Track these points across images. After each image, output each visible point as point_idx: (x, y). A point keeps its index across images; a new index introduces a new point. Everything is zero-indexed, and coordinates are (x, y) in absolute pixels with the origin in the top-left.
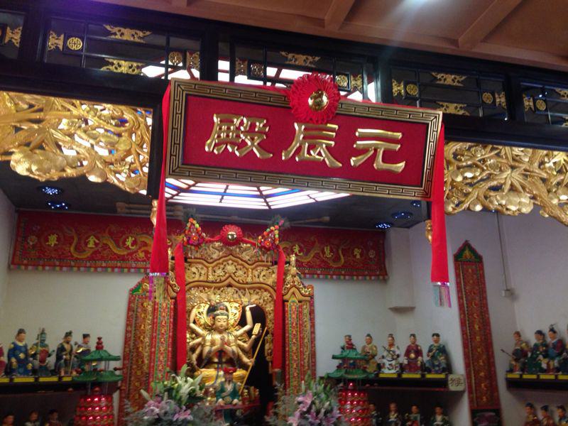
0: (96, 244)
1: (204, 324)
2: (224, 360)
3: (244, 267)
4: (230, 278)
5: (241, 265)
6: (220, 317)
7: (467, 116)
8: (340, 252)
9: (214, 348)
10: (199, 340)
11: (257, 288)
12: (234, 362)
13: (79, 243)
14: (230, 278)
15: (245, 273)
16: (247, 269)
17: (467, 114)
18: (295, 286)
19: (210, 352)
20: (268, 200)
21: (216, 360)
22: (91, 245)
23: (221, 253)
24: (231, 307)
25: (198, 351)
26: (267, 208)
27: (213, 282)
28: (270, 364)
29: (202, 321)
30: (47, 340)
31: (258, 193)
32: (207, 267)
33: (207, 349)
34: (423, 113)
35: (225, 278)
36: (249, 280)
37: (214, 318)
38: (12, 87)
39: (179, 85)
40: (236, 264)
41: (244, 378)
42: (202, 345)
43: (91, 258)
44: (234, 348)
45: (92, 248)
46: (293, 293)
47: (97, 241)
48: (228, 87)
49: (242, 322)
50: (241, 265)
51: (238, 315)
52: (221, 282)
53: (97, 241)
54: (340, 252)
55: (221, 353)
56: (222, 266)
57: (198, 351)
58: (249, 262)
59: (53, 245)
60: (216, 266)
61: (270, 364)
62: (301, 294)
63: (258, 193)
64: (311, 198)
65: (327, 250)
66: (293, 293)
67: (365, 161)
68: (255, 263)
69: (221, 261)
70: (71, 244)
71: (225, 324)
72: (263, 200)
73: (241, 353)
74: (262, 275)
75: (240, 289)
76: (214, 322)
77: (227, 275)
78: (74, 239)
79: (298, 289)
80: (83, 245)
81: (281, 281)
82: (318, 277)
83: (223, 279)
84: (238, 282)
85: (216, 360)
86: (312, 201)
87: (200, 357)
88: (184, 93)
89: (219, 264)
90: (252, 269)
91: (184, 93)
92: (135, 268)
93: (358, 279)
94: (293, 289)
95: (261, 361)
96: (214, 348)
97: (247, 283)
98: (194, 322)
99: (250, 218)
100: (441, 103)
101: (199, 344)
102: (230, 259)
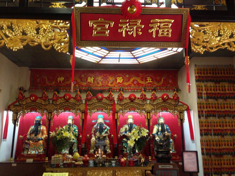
7: (207, 10)
17: (207, 9)
20: (138, 59)
26: (138, 63)
31: (133, 57)
34: (144, 10)
38: (211, 20)
39: (77, 9)
48: (157, 9)
63: (133, 57)
64: (155, 57)
67: (99, 37)
72: (136, 60)
78: (81, 3)
82: (164, 90)
86: (156, 59)
88: (79, 12)
91: (184, 14)
92: (148, 89)
93: (169, 91)
99: (134, 69)
100: (194, 6)
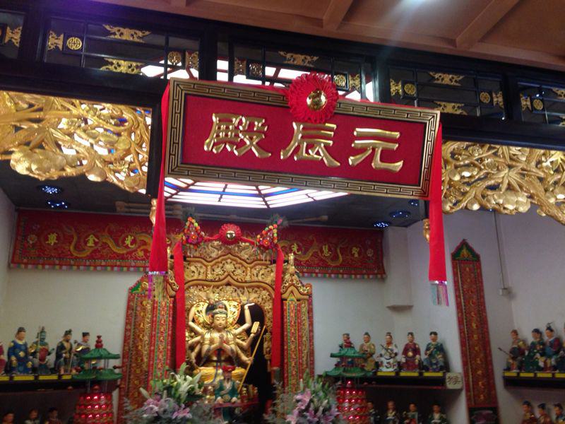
0: (96, 243)
1: (203, 323)
2: (223, 358)
3: (243, 266)
4: (229, 277)
5: (240, 263)
6: (219, 315)
7: (465, 115)
8: (338, 251)
9: (213, 346)
10: (198, 338)
11: (256, 287)
12: (233, 360)
13: (78, 242)
14: (229, 277)
15: (244, 272)
16: (246, 268)
17: (465, 113)
18: (293, 285)
19: (208, 351)
20: (267, 199)
21: (215, 358)
22: (91, 244)
23: (220, 252)
24: (230, 306)
25: (197, 350)
26: (266, 207)
27: (211, 281)
28: (269, 362)
29: (201, 320)
30: (47, 338)
31: (257, 192)
32: (206, 266)
33: (206, 347)
34: (421, 113)
35: (223, 276)
36: (248, 278)
37: (213, 317)
38: (12, 87)
39: (178, 85)
40: (235, 263)
41: (242, 376)
42: (201, 343)
43: (91, 257)
44: (233, 347)
45: (91, 247)
46: (292, 292)
47: (97, 240)
48: (227, 86)
49: (241, 320)
50: (240, 263)
51: (237, 314)
52: (220, 280)
53: (97, 240)
54: (338, 251)
55: (220, 351)
56: (221, 265)
57: (197, 350)
58: (247, 261)
59: (52, 244)
60: (215, 264)
61: (269, 362)
62: (300, 292)
63: (257, 192)
64: (309, 197)
65: (326, 249)
66: (292, 292)
67: (364, 160)
68: (254, 261)
69: (220, 260)
70: (70, 243)
71: (223, 322)
72: (261, 199)
73: (240, 352)
74: (261, 273)
75: (238, 287)
76: (213, 320)
77: (226, 274)
78: (73, 238)
79: (297, 288)
80: (83, 244)
81: (279, 280)
82: (317, 276)
83: (222, 277)
84: (237, 281)
85: (215, 358)
86: (311, 200)
87: (199, 356)
88: (184, 92)
89: (218, 262)
90: (251, 268)
91: (184, 92)
92: (134, 267)
93: (356, 277)
94: (292, 288)
95: (259, 359)
96: (213, 346)
97: (246, 282)
98: (193, 321)
99: (248, 217)
100: (439, 103)
101: (198, 342)
102: (229, 258)
